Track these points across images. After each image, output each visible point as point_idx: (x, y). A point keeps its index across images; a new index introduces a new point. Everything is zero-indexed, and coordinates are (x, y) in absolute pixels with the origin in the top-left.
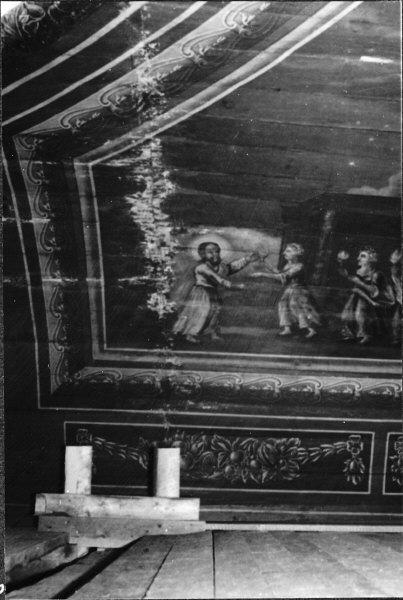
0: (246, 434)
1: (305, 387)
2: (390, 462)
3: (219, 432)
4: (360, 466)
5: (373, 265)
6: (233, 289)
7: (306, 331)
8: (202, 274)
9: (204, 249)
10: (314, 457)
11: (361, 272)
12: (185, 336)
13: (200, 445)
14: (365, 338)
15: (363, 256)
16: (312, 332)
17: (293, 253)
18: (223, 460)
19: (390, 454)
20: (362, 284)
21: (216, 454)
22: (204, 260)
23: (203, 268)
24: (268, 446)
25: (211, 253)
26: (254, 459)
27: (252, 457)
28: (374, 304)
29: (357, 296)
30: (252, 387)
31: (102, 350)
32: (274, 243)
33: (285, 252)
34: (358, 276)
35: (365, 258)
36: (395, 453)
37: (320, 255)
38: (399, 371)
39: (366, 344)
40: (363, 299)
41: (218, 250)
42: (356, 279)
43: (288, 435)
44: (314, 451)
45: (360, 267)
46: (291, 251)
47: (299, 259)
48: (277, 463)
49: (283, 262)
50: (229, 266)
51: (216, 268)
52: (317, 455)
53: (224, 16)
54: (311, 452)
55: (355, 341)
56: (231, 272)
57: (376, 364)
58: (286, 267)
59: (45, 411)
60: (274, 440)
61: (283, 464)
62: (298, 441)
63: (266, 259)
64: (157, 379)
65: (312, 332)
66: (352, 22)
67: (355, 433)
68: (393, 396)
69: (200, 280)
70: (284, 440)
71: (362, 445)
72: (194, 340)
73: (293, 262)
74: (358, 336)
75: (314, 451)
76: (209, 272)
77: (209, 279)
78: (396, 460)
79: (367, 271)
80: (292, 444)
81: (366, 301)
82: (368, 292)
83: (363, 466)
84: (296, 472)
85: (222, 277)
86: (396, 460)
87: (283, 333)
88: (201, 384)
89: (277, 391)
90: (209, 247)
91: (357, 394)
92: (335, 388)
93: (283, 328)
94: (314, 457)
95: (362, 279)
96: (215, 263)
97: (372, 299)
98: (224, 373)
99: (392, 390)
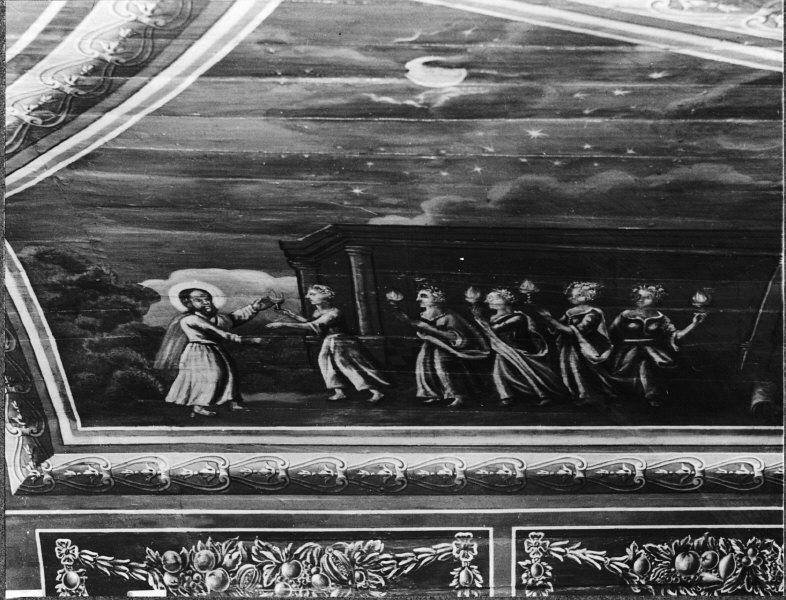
0: (697, 533)
1: (381, 468)
2: (520, 570)
3: (264, 536)
4: (475, 577)
5: (443, 307)
6: (244, 344)
7: (366, 394)
8: (195, 327)
9: (189, 297)
10: (404, 567)
11: (428, 314)
12: (192, 407)
13: (235, 556)
14: (457, 399)
15: (423, 296)
16: (376, 395)
17: (321, 296)
18: (273, 575)
19: (519, 559)
20: (435, 330)
21: (260, 568)
22: (192, 311)
23: (193, 319)
24: (337, 553)
25: (199, 301)
26: (317, 572)
27: (314, 570)
28: (460, 355)
29: (431, 348)
30: (304, 472)
31: (74, 431)
32: (289, 283)
33: (308, 296)
34: (425, 321)
35: (427, 299)
36: (527, 557)
37: (427, 302)
38: (781, 441)
39: (459, 407)
40: (442, 350)
41: (210, 297)
42: (422, 324)
43: (366, 536)
44: (405, 558)
45: (424, 309)
46: (315, 295)
47: (328, 303)
48: (351, 577)
49: (308, 310)
50: (231, 316)
51: (213, 320)
52: (409, 564)
53: (78, 40)
54: (417, 554)
55: (440, 403)
56: (235, 324)
57: (482, 433)
58: (316, 314)
59: (488, 526)
60: (344, 543)
61: (361, 579)
62: (379, 545)
63: (283, 307)
64: (637, 468)
65: (376, 395)
66: (261, 43)
67: (463, 530)
68: (216, 476)
69: (192, 335)
70: (360, 543)
71: (475, 547)
72: (207, 413)
73: (323, 308)
74: (446, 397)
75: (405, 558)
76: (204, 325)
77: (207, 334)
78: (529, 566)
79: (435, 315)
80: (371, 550)
81: (447, 352)
82: (447, 341)
83: (480, 577)
84: (380, 588)
85: (225, 330)
86: (529, 566)
87: (335, 398)
88: (286, 471)
89: (340, 475)
90: (194, 294)
91: (460, 476)
92: (544, 469)
93: (332, 391)
94: (404, 567)
95: (433, 323)
96: (210, 313)
97: (455, 348)
98: (259, 454)
99: (572, 468)
